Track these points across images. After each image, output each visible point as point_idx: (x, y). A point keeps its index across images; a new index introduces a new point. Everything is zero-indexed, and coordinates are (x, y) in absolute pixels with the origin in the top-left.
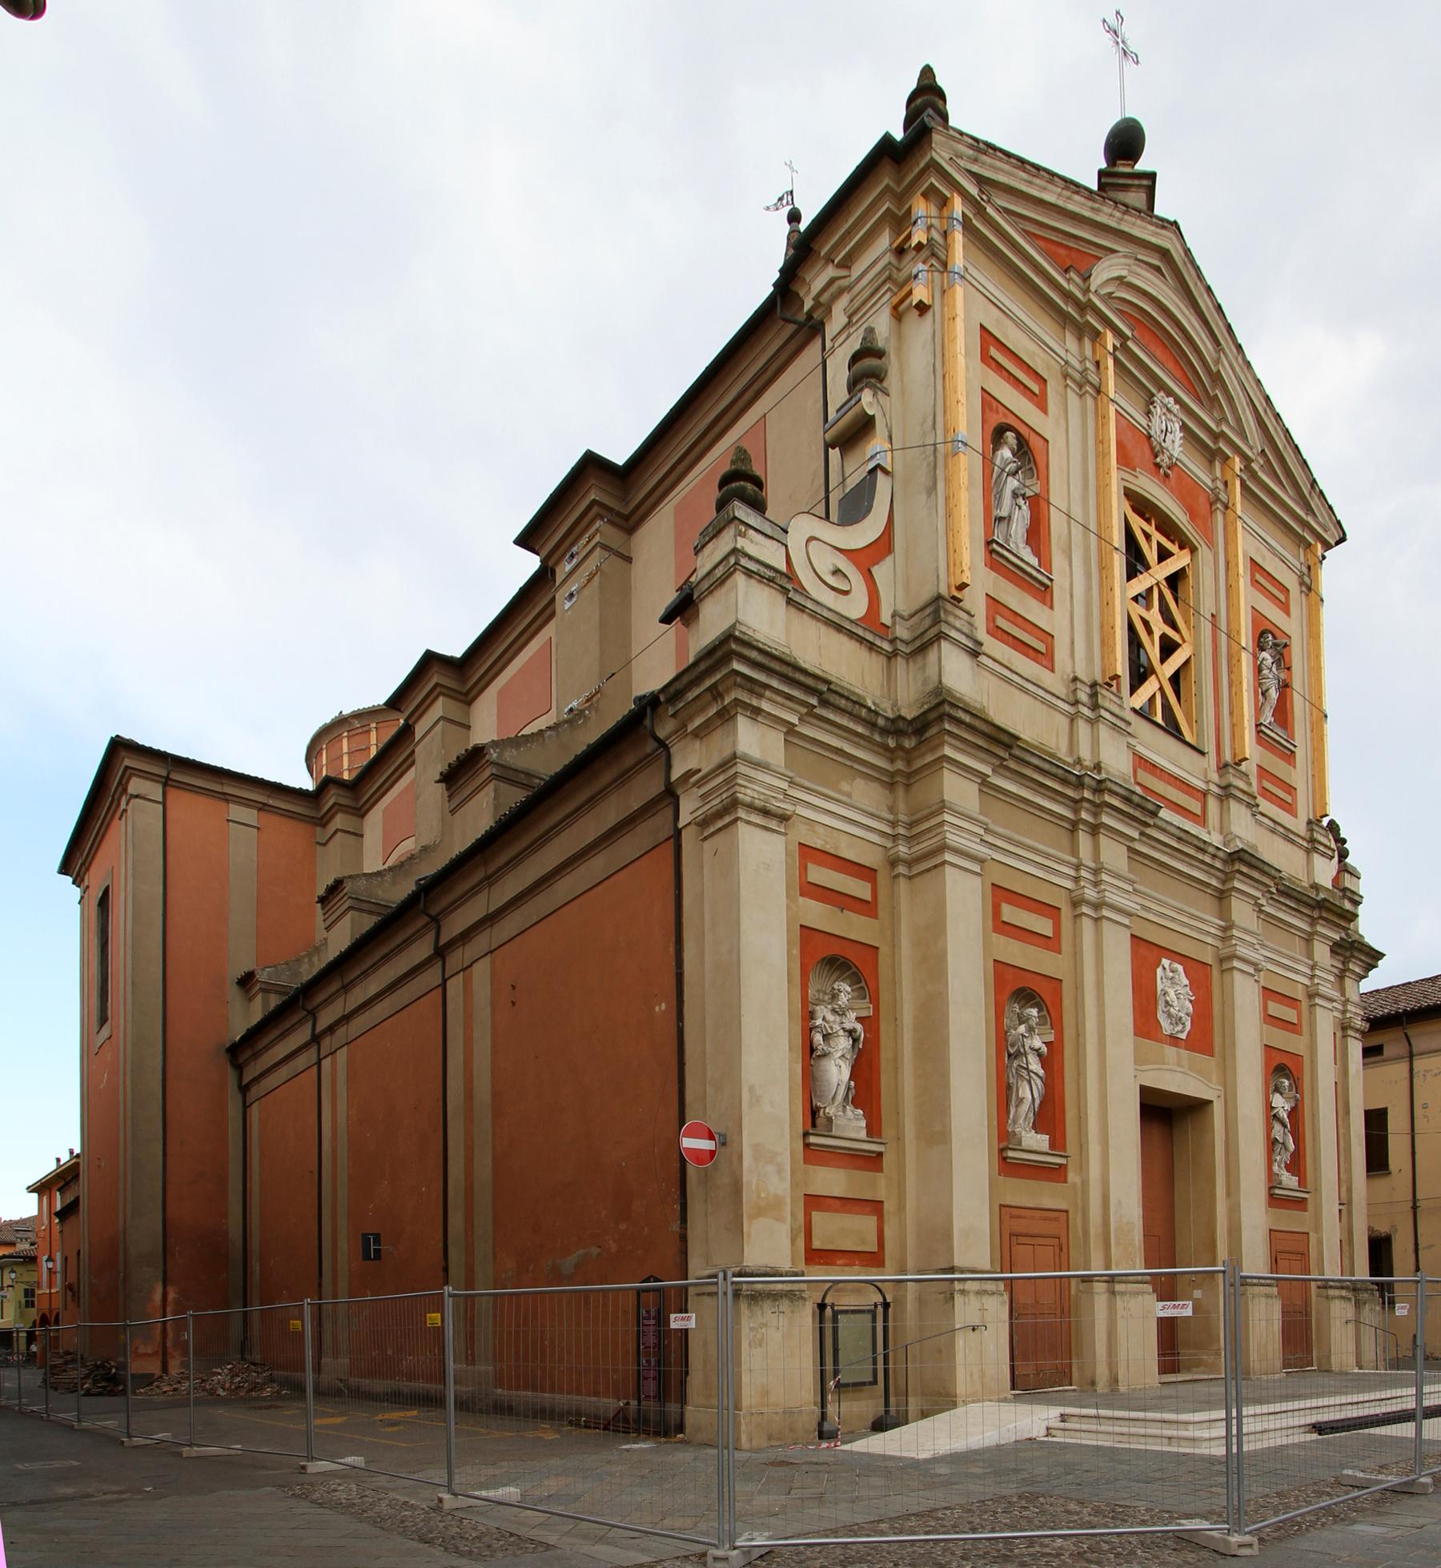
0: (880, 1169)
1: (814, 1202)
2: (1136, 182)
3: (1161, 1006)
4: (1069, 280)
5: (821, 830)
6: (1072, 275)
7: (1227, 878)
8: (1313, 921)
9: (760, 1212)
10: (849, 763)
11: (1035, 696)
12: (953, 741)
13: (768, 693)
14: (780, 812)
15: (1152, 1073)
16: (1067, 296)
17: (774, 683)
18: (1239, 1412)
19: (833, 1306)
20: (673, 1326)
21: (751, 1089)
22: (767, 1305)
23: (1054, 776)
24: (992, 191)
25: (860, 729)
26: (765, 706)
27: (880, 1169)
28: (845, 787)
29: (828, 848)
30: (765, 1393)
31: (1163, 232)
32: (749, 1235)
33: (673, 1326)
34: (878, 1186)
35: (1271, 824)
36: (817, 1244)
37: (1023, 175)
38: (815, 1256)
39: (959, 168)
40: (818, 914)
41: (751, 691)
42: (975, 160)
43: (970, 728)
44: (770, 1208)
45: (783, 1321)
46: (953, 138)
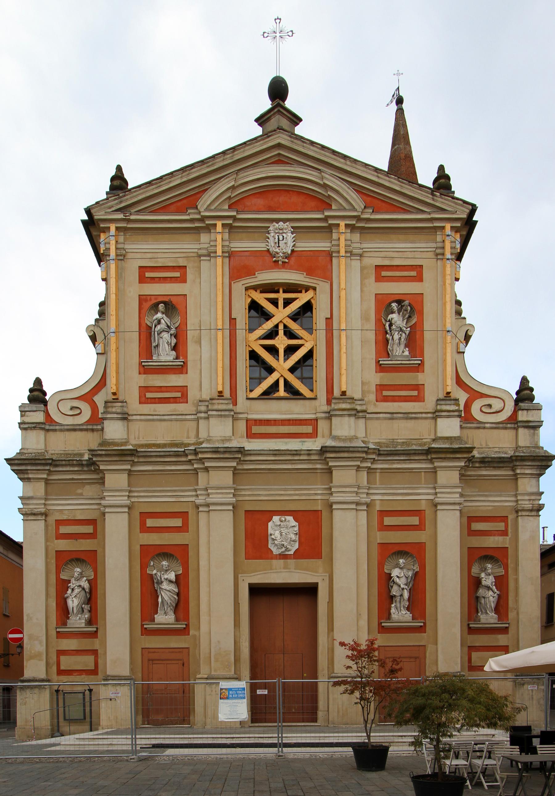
0: (97, 637)
1: (61, 653)
2: (272, 113)
3: (270, 541)
4: (189, 214)
5: (66, 512)
6: (189, 211)
7: (325, 461)
8: (431, 461)
9: (31, 658)
10: (81, 481)
11: (171, 420)
12: (102, 463)
13: (29, 472)
14: (39, 512)
15: (259, 576)
16: (192, 221)
17: (29, 468)
18: (135, 736)
19: (62, 691)
20: (258, 693)
21: (28, 615)
22: (28, 691)
23: (170, 456)
24: (128, 209)
25: (76, 469)
26: (31, 476)
27: (97, 637)
28: (79, 491)
29: (70, 518)
30: (26, 721)
31: (270, 138)
32: (26, 666)
33: (258, 693)
34: (96, 644)
35: (388, 415)
36: (62, 668)
37: (154, 187)
38: (60, 672)
39: (109, 213)
40: (63, 545)
41: (23, 473)
42: (121, 202)
43: (106, 455)
44: (37, 656)
45: (35, 696)
46: (103, 204)
